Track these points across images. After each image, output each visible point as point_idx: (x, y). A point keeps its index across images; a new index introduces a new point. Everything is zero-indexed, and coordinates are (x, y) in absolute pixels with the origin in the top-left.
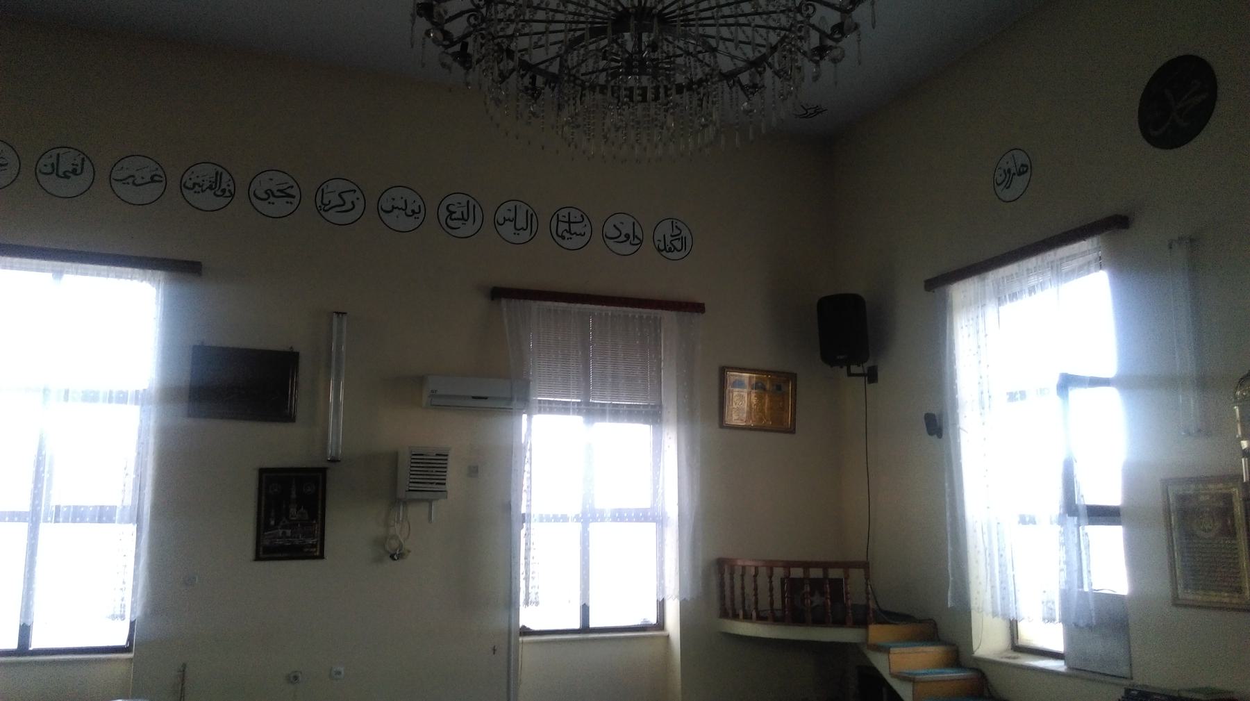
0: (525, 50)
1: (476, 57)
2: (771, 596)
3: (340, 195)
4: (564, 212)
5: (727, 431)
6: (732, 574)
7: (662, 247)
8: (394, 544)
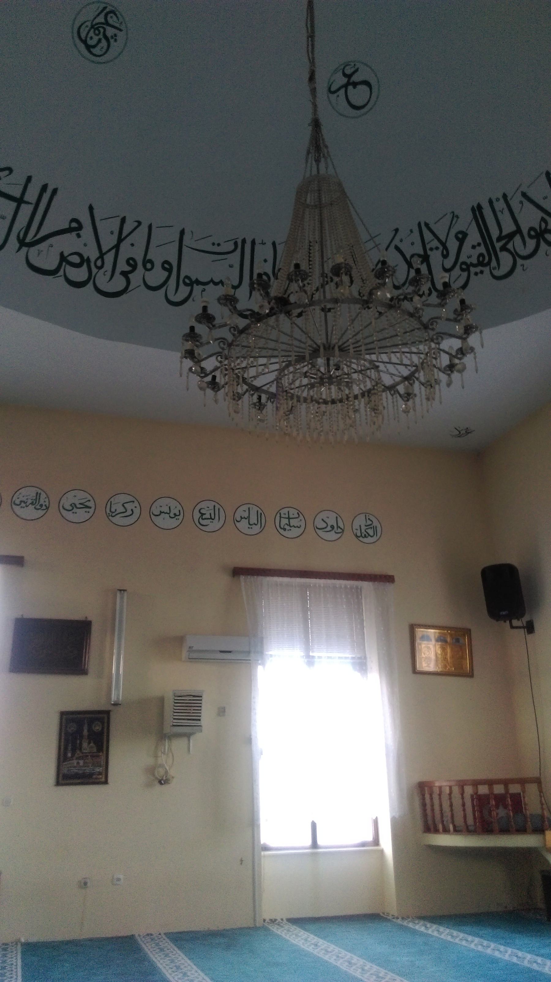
0: (251, 367)
1: (222, 383)
2: (464, 810)
3: (123, 506)
4: (286, 511)
5: (418, 676)
6: (431, 795)
7: (359, 534)
8: (161, 771)
